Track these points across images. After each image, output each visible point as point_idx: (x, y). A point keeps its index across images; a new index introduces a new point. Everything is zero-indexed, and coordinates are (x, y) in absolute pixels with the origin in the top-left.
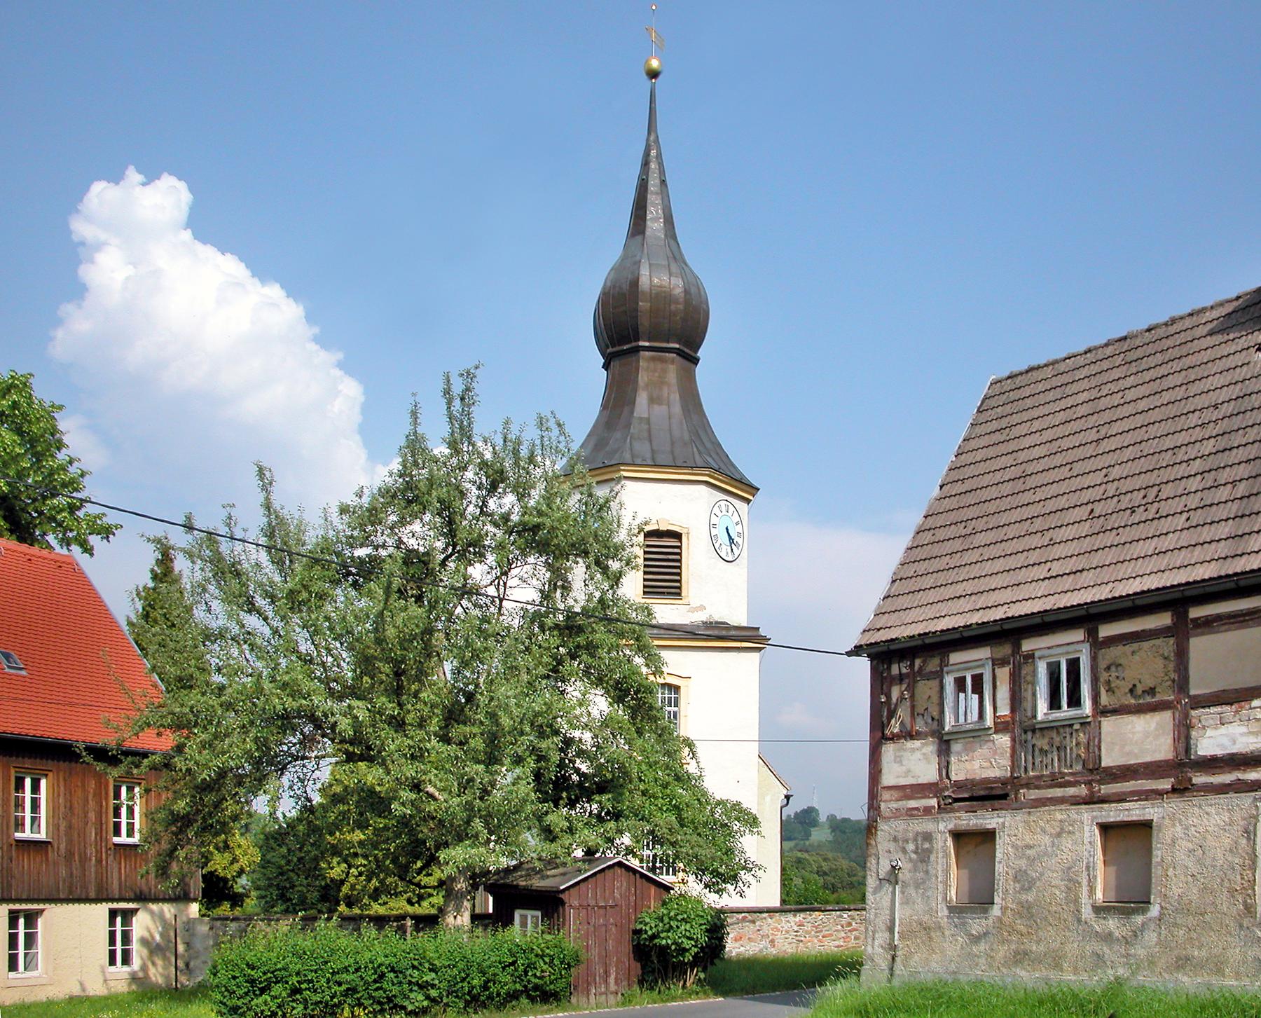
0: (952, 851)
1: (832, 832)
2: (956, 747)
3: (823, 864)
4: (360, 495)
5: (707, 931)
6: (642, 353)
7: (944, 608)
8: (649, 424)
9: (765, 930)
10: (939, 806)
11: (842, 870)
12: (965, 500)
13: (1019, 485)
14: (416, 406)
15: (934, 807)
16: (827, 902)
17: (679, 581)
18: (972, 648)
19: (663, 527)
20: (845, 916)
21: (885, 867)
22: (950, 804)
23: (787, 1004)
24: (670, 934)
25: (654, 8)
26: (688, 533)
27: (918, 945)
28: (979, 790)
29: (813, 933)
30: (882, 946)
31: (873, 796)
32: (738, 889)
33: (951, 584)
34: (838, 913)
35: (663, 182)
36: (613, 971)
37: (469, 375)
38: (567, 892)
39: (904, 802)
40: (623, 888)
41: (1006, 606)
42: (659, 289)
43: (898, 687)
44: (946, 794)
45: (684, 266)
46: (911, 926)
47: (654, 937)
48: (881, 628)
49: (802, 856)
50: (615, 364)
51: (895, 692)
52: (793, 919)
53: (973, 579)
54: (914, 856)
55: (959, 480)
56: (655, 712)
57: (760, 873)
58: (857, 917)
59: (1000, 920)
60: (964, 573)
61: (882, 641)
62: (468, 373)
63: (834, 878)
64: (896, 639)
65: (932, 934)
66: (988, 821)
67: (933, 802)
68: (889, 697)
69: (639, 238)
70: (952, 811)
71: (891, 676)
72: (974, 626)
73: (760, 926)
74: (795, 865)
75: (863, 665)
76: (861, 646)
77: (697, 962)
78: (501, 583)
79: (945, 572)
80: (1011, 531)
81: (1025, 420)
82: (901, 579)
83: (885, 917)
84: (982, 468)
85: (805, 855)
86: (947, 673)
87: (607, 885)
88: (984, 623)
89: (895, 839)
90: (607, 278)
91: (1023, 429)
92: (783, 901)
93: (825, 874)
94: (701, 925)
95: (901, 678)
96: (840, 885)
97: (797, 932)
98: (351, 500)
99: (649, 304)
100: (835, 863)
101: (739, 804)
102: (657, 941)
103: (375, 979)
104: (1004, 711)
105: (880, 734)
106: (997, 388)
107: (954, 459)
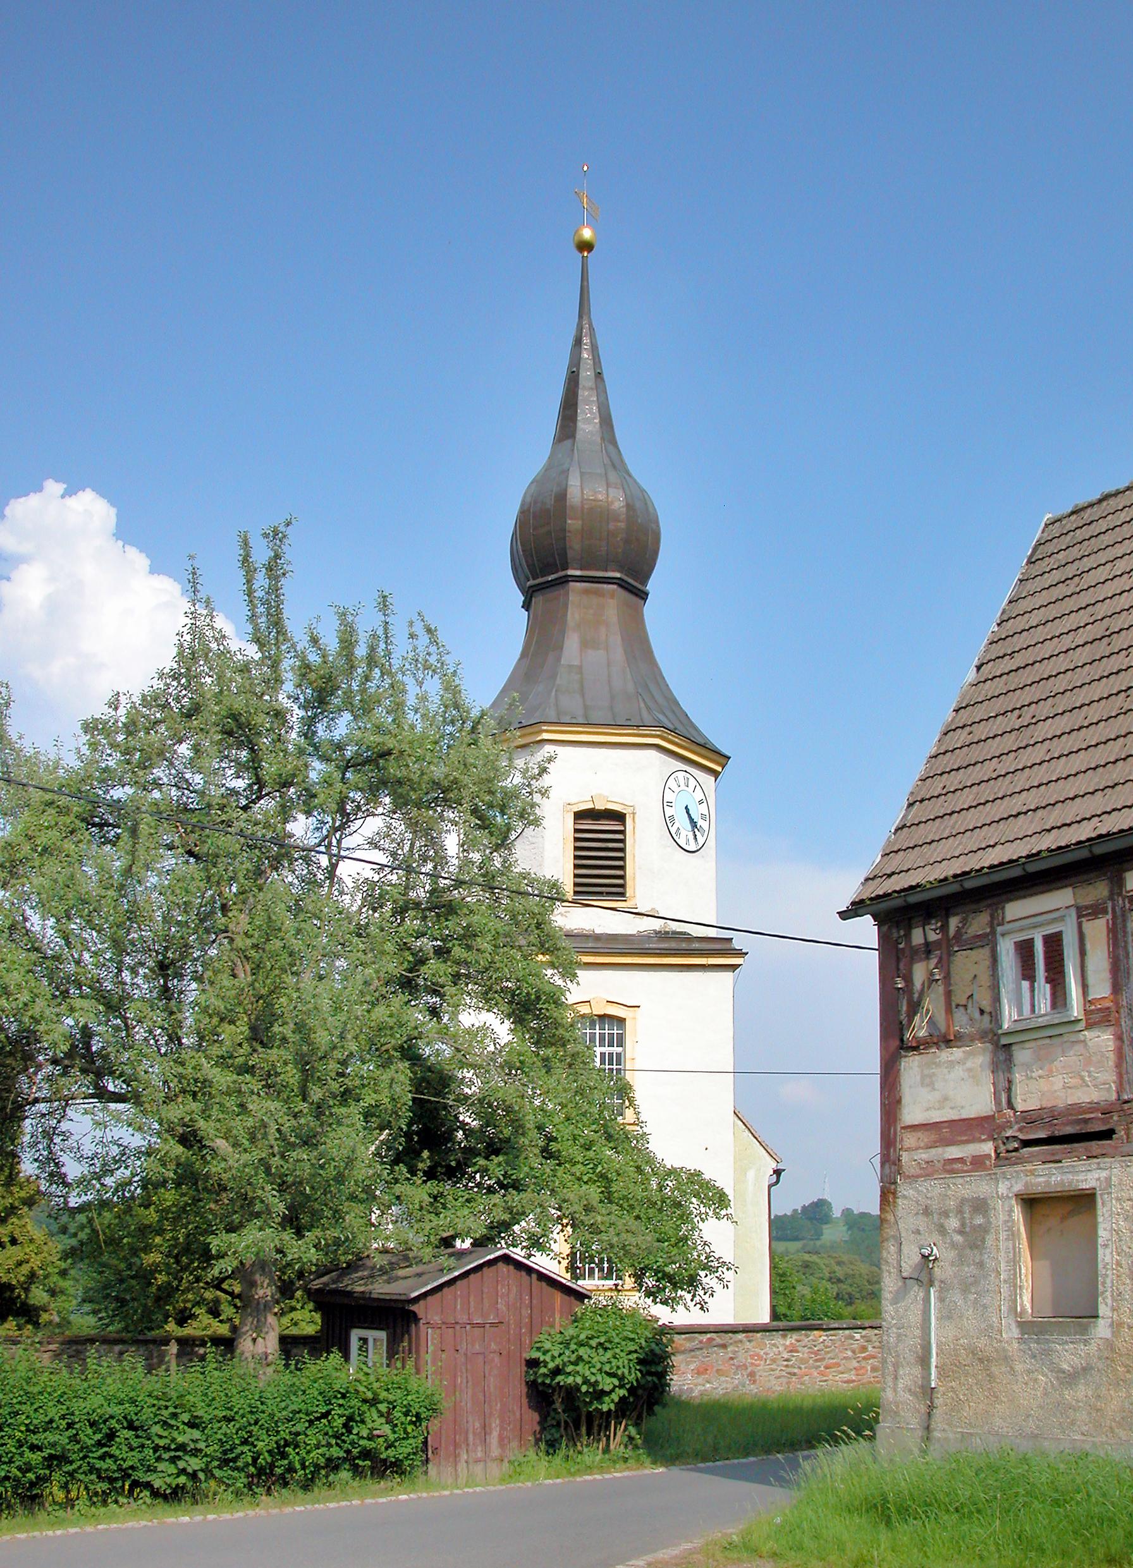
0: (1022, 1229)
1: (849, 1229)
2: (1021, 1055)
3: (837, 1268)
4: (114, 704)
5: (640, 1362)
6: (571, 584)
7: (992, 835)
8: (581, 673)
9: (742, 1358)
10: (998, 1155)
11: (860, 1275)
12: (1016, 680)
13: (1102, 648)
14: (194, 574)
15: (990, 1155)
16: (839, 1317)
17: (623, 877)
18: (1042, 892)
19: (600, 806)
20: (857, 1336)
21: (911, 1258)
22: (1016, 1150)
23: (765, 1481)
24: (578, 1368)
25: (585, 168)
26: (634, 814)
27: (970, 1388)
28: (1063, 1124)
29: (811, 1362)
30: (910, 1390)
31: (889, 1141)
32: (697, 1299)
33: (1002, 798)
34: (847, 1332)
35: (599, 375)
36: (495, 1423)
37: (276, 536)
38: (422, 1302)
39: (940, 1150)
40: (512, 1296)
41: (1096, 819)
42: (594, 503)
43: (924, 963)
44: (1009, 1133)
45: (627, 477)
46: (957, 1355)
47: (557, 1371)
48: (893, 873)
49: (810, 1259)
50: (538, 600)
51: (919, 972)
52: (782, 1341)
53: (1038, 787)
54: (958, 1238)
55: (1005, 655)
56: (561, 1031)
57: (728, 1275)
58: (874, 1338)
59: (1110, 1345)
60: (1021, 780)
61: (895, 891)
62: (276, 532)
63: (851, 1285)
64: (918, 886)
65: (993, 1368)
66: (1081, 1177)
67: (988, 1148)
68: (908, 979)
69: (568, 443)
70: (1021, 1161)
71: (912, 947)
72: (1044, 854)
73: (735, 1352)
74: (802, 1270)
75: (866, 929)
76: (862, 901)
77: (623, 1409)
78: (334, 842)
79: (992, 782)
80: (1094, 713)
81: (1103, 562)
82: (921, 801)
83: (913, 1340)
84: (1040, 634)
85: (814, 1258)
86: (1003, 935)
87: (486, 1290)
88: (1060, 848)
89: (927, 1212)
90: (525, 493)
91: (1102, 573)
92: (775, 1316)
93: (839, 1281)
94: (630, 1352)
95: (928, 949)
96: (858, 1296)
97: (786, 1360)
98: (100, 710)
99: (580, 522)
100: (852, 1267)
101: (698, 1174)
102: (559, 1378)
103: (99, 1441)
104: (1101, 989)
105: (897, 1043)
106: (1056, 530)
107: (996, 629)
